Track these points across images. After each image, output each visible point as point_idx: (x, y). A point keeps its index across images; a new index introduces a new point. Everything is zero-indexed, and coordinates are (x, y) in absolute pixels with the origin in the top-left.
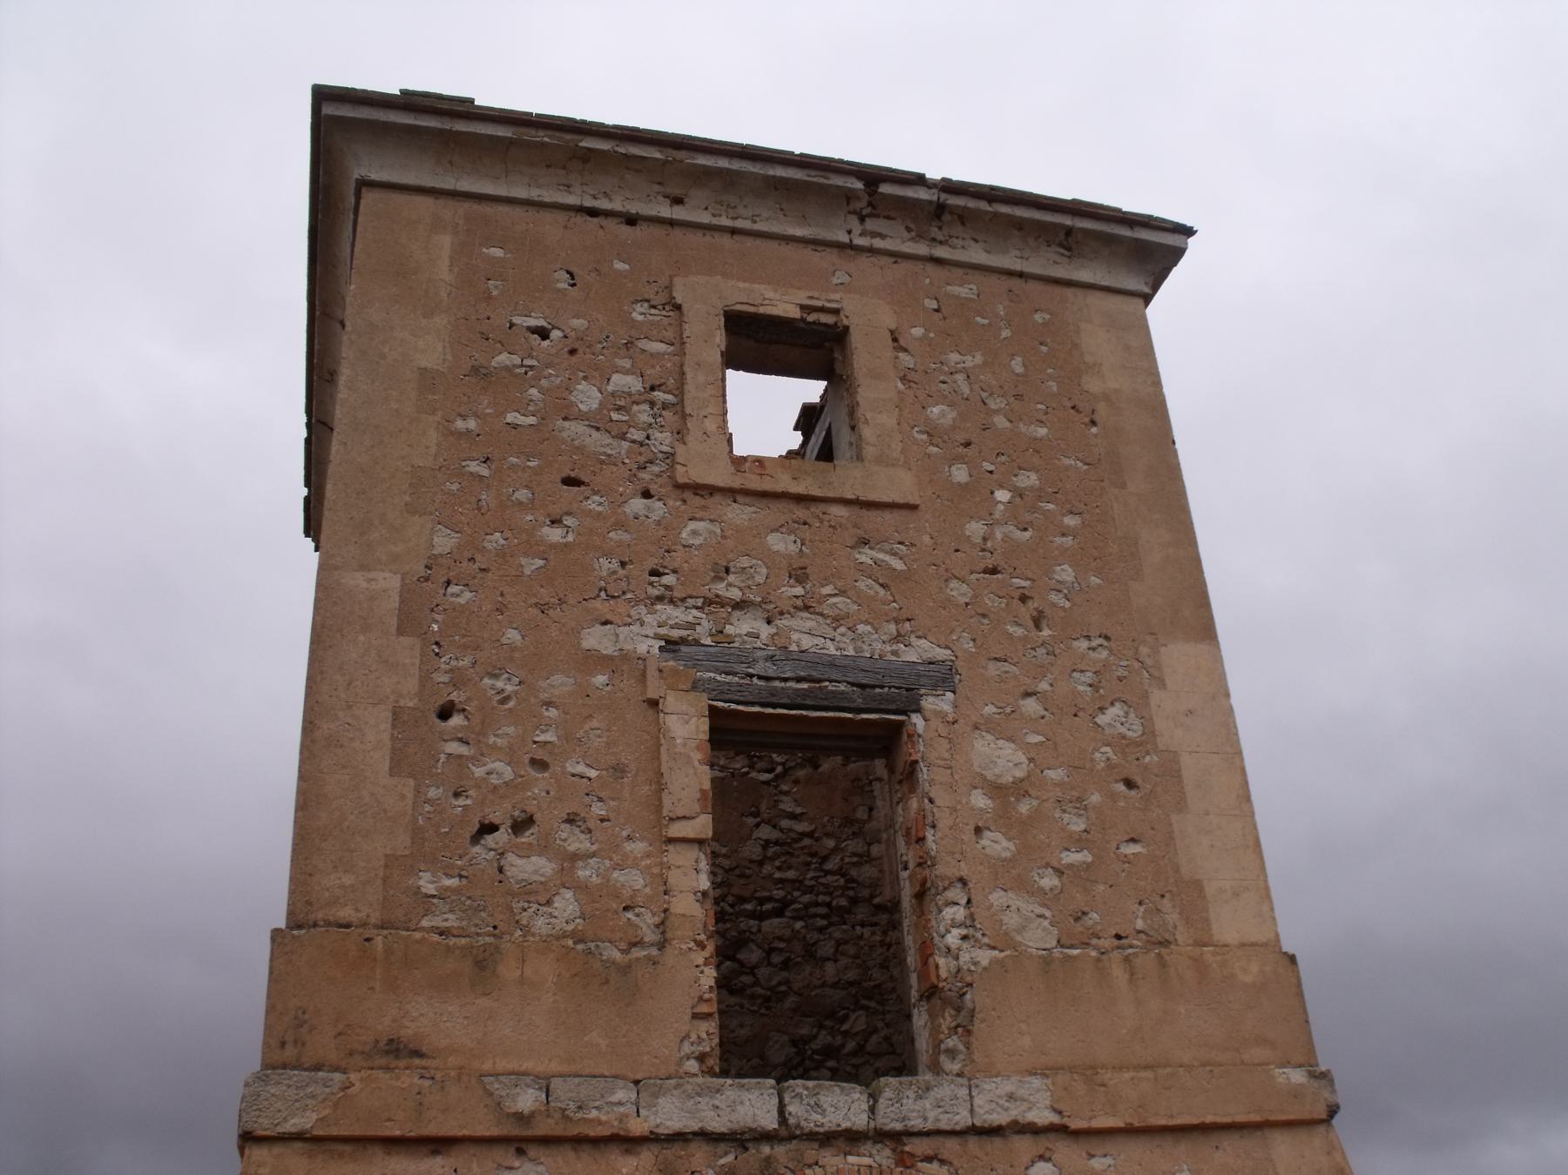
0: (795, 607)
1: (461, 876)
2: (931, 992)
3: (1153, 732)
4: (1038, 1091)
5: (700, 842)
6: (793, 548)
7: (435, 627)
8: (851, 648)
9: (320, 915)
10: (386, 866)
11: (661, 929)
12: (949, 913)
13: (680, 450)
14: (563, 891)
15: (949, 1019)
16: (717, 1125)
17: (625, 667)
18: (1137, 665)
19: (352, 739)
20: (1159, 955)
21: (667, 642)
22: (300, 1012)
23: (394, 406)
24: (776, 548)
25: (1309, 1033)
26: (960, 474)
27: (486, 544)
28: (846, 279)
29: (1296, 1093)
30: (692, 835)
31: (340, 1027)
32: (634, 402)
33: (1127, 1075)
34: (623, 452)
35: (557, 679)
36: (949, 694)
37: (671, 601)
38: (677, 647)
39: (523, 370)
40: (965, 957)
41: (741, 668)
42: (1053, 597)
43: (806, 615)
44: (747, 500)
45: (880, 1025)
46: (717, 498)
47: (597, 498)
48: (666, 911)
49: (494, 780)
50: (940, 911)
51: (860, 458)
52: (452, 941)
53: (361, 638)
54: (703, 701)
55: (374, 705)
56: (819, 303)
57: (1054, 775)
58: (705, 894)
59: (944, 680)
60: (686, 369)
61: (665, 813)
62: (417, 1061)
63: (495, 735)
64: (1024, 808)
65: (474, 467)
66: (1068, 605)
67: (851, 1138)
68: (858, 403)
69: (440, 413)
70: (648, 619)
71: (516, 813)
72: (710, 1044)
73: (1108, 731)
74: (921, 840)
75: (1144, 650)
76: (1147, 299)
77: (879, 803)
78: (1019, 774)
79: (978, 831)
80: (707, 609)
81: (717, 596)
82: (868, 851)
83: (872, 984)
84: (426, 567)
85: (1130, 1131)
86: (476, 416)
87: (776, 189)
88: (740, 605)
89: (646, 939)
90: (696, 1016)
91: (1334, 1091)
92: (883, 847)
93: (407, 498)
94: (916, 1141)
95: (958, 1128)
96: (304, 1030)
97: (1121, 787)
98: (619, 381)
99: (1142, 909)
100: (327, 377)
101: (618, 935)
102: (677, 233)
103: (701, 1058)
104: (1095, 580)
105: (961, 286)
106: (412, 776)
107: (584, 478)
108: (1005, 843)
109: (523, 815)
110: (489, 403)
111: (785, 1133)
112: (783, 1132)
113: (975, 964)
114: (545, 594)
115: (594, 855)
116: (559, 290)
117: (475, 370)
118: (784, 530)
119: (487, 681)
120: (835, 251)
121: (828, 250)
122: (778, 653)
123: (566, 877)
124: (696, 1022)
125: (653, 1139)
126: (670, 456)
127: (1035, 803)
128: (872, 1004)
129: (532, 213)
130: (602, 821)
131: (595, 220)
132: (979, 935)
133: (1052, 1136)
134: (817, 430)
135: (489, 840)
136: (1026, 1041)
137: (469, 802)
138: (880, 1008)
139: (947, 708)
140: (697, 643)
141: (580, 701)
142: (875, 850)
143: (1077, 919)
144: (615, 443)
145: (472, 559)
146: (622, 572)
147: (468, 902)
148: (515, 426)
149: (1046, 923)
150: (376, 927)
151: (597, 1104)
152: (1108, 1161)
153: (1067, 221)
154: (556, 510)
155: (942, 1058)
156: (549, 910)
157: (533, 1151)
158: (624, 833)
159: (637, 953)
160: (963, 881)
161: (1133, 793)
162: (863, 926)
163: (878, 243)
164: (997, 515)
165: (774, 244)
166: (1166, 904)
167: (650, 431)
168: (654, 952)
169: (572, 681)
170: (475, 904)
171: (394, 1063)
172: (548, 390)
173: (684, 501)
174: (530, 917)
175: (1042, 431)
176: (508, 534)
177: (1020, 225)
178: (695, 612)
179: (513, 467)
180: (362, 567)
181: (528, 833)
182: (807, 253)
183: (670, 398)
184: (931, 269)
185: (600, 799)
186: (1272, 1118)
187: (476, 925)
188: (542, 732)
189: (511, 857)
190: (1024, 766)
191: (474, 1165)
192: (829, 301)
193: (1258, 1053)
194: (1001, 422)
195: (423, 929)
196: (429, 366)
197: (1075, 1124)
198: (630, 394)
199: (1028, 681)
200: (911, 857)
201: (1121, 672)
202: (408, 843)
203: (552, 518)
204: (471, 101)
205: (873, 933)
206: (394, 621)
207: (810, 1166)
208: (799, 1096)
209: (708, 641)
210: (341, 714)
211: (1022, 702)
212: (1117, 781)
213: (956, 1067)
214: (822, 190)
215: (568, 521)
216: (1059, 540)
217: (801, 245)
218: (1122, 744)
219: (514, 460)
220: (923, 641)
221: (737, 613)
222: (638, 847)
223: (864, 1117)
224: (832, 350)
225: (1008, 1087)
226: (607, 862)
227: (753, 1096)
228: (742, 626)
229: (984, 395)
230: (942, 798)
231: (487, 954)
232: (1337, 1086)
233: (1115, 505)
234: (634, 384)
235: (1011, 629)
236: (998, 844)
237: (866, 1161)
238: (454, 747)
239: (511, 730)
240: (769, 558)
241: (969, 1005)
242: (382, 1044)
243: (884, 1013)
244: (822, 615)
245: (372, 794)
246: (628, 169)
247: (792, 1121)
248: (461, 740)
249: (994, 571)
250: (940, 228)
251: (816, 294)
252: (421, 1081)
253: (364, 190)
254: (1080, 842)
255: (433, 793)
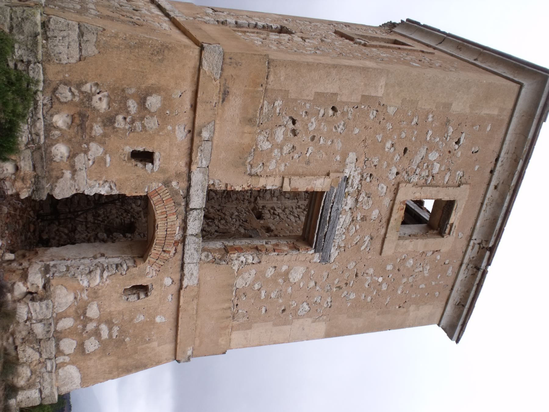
0: (353, 217)
1: (279, 113)
2: (227, 250)
3: (299, 318)
4: (193, 282)
5: (282, 187)
6: (373, 217)
7: (363, 107)
8: (338, 233)
9: (272, 70)
10: (285, 90)
11: (255, 174)
12: (250, 258)
13: (411, 185)
14: (271, 145)
15: (218, 256)
16: (192, 191)
17: (341, 166)
18: (320, 315)
19: (329, 80)
20: (230, 317)
21: (348, 178)
22: (240, 64)
23: (440, 95)
24: (374, 212)
25: (202, 356)
26: (389, 267)
27: (388, 124)
28: (460, 237)
29: (184, 352)
30: (284, 185)
31: (234, 77)
32: (429, 171)
33: (195, 307)
34: (413, 167)
35: (340, 145)
36: (319, 261)
37: (361, 180)
38: (346, 181)
39: (446, 136)
40: (236, 262)
41: (336, 200)
42: (345, 293)
43: (351, 220)
44: (391, 204)
45: (218, 196)
46: (393, 195)
47: (399, 158)
48: (261, 176)
49: (310, 124)
50: (251, 255)
51: (400, 238)
52: (259, 112)
53: (362, 84)
54: (327, 189)
55: (339, 87)
56: (453, 229)
57: (289, 290)
58: (265, 187)
59: (324, 260)
60: (438, 188)
61: (292, 177)
62: (221, 100)
63: (324, 125)
64: (280, 281)
65: (415, 120)
66: (342, 296)
67: (184, 229)
68: (417, 239)
69: (435, 110)
70: (356, 173)
71: (298, 131)
72: (217, 187)
73: (301, 305)
74: (274, 251)
75: (325, 317)
76: (439, 325)
77: (290, 201)
78: (291, 280)
79: (275, 267)
80: (357, 190)
81: (361, 194)
82: (275, 197)
83: (232, 195)
84: (383, 105)
85: (178, 307)
86: (432, 121)
87: (494, 219)
88: (357, 200)
89: (253, 169)
90: (227, 185)
91: (184, 362)
92: (276, 201)
93: (408, 99)
94: (182, 247)
95: (184, 259)
96: (235, 65)
97: (283, 308)
98: (437, 166)
99: (245, 312)
100: (459, 47)
101: (255, 161)
102: (485, 186)
103: (213, 184)
104: (349, 304)
105: (452, 271)
106: (314, 99)
107: (406, 154)
108: (270, 275)
109: (297, 133)
110: (436, 125)
111: (188, 210)
112: (188, 209)
113: (234, 265)
114: (369, 142)
115: (282, 154)
116: (472, 148)
117: (448, 121)
118: (379, 215)
119: (342, 123)
120: (470, 234)
121: (471, 232)
122: (340, 211)
123: (275, 146)
124: (225, 184)
125: (190, 171)
126: (409, 182)
127: (281, 284)
128: (225, 194)
129: (501, 140)
130: (292, 157)
131: (494, 160)
132: (243, 266)
133: (179, 285)
134: (415, 205)
135: (290, 122)
136: (208, 279)
137: (303, 116)
138: (223, 197)
139: (315, 260)
140: (346, 187)
141: (332, 151)
142: (275, 199)
143: (244, 294)
144: (417, 164)
145: (384, 119)
146: (373, 165)
147: (271, 116)
148: (427, 134)
149: (244, 285)
150: (266, 87)
151: (202, 156)
152: (170, 300)
153: (467, 306)
154: (397, 146)
155: (206, 253)
156: (265, 141)
157: (189, 135)
158: (287, 164)
159: (248, 167)
160: (260, 262)
161: (281, 311)
162: (251, 193)
163: (470, 248)
164: (374, 278)
165: (476, 216)
166: (246, 319)
167: (418, 175)
168: (249, 172)
169: (339, 149)
170: (270, 118)
171: (221, 93)
172: (438, 144)
173: (393, 185)
174: (264, 135)
175: (399, 292)
176: (391, 131)
177: (468, 292)
178: (356, 187)
179: (413, 132)
180: (386, 84)
181: (291, 134)
182: (471, 225)
183: (429, 182)
184: (459, 262)
185: (299, 157)
186: (178, 345)
187: (263, 118)
188: (324, 140)
189: (284, 129)
190: (293, 281)
191: (187, 118)
192: (453, 232)
193: (197, 342)
194: (405, 280)
195: (264, 101)
196: (452, 106)
197: (182, 292)
198: (432, 169)
199: (320, 284)
200: (269, 246)
201: (319, 310)
202: (292, 97)
203: (394, 145)
204: (545, 121)
205: (248, 196)
206: (366, 94)
207: (177, 216)
208: (199, 214)
209: (346, 190)
210: (338, 77)
211: (313, 281)
212: (285, 307)
213: (203, 258)
214: (491, 234)
215: (392, 149)
216: (363, 295)
217: (474, 224)
218: (296, 309)
219: (416, 132)
220: (337, 254)
221: (354, 199)
222: (282, 168)
223: (191, 233)
224: (437, 230)
225: (195, 273)
226: (278, 158)
227: (200, 201)
228: (350, 201)
229: (414, 276)
230: (286, 258)
231: (253, 122)
232: (185, 363)
233: (372, 312)
234: (436, 170)
235: (337, 280)
236: (270, 272)
237: (177, 232)
238: (322, 112)
239: (325, 130)
240: (371, 210)
241: (221, 263)
242: (228, 89)
243: (222, 198)
244: (350, 225)
245: (310, 86)
246: (510, 173)
247: (191, 212)
248: (324, 114)
249: (356, 275)
250: (472, 267)
251: (456, 228)
252: (214, 103)
253: (519, 86)
254: (268, 296)
255: (308, 105)
